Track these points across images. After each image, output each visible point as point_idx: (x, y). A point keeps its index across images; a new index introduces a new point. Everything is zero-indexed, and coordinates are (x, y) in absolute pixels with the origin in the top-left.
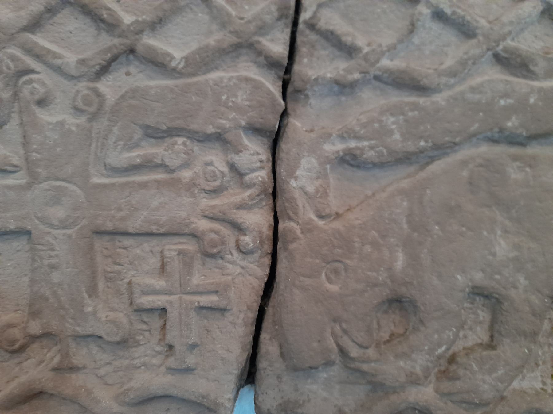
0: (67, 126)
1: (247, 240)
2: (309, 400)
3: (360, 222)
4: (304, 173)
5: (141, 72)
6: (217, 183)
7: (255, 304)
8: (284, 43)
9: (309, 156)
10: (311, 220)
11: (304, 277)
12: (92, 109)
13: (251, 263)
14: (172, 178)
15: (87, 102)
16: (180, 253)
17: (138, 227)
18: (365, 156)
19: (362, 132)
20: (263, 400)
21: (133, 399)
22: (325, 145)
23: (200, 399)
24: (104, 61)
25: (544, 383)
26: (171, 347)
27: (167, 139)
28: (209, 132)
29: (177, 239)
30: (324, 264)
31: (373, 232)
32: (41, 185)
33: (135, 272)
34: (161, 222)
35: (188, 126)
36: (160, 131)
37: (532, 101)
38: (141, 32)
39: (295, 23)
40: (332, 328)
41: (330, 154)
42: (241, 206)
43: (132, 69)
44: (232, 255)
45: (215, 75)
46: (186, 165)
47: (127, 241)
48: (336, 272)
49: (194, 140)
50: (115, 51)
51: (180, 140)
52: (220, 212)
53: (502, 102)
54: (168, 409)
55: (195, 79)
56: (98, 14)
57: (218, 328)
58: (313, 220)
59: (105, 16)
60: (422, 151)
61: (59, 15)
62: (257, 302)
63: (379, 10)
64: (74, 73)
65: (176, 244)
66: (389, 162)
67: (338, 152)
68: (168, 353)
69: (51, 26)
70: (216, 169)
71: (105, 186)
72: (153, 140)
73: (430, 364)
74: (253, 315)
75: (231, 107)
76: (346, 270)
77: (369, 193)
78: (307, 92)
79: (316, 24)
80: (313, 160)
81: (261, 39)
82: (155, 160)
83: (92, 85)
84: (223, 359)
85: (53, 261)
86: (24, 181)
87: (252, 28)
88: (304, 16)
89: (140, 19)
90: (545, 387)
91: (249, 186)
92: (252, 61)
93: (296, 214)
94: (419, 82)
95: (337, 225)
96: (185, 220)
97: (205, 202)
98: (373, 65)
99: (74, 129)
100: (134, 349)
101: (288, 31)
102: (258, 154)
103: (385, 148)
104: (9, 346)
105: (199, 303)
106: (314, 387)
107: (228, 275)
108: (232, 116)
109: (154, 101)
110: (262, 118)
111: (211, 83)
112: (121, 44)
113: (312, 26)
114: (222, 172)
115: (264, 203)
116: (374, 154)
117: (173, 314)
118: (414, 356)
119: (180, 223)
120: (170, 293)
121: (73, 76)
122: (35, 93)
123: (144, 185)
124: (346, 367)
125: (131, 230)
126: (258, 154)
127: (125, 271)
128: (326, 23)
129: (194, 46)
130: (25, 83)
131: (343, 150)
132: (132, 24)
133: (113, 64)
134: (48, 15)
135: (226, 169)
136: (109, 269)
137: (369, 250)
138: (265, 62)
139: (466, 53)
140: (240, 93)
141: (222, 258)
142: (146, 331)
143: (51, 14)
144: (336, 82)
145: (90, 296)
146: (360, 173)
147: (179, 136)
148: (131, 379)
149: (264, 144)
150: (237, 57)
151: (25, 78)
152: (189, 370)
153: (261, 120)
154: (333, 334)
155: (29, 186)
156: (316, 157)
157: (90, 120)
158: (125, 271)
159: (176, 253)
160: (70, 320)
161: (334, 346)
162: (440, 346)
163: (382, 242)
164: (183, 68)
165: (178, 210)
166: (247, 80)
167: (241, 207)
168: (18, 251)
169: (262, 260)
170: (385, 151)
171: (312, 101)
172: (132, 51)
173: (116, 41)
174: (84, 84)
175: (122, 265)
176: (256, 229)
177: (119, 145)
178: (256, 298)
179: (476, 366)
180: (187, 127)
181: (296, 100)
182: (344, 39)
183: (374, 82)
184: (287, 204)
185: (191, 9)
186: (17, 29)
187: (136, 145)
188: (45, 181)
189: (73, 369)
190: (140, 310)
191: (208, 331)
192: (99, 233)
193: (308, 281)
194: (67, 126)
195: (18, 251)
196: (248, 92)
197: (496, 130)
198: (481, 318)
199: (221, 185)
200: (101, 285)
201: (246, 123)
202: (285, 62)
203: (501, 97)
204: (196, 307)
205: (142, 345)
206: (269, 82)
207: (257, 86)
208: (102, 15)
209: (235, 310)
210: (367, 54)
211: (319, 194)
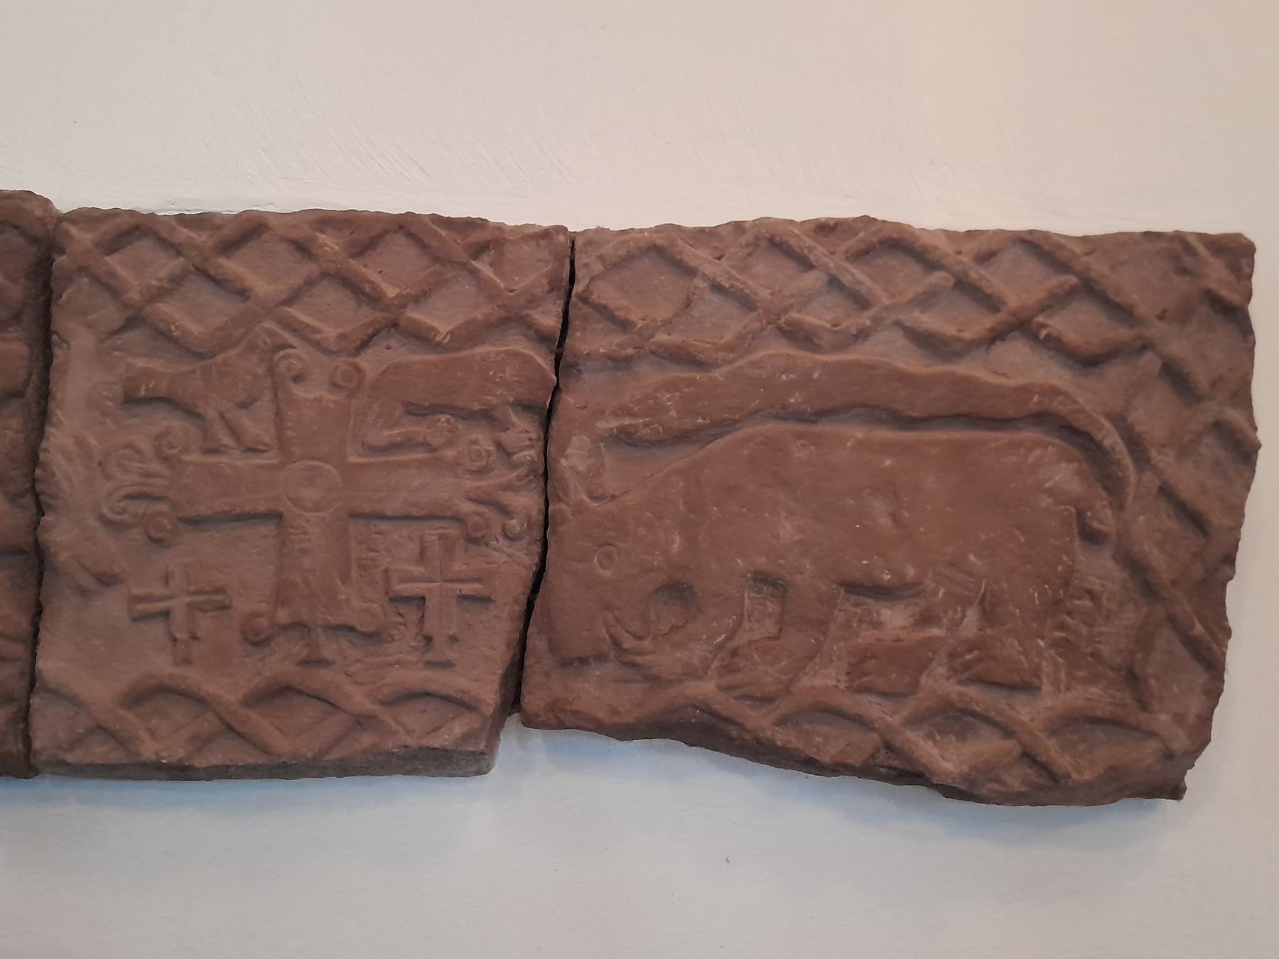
0: (325, 403)
1: (514, 523)
5: (403, 345)
6: (483, 463)
7: (522, 597)
10: (583, 500)
12: (351, 386)
13: (519, 551)
16: (441, 537)
18: (639, 434)
19: (636, 409)
25: (838, 681)
26: (429, 639)
27: (429, 417)
28: (475, 409)
29: (438, 524)
30: (595, 548)
31: (648, 513)
32: (295, 465)
37: (816, 376)
38: (405, 306)
39: (569, 296)
43: (393, 343)
44: (497, 540)
45: (481, 350)
46: (449, 443)
47: (384, 526)
49: (459, 418)
50: (377, 326)
51: (444, 418)
53: (784, 377)
54: (424, 711)
55: (463, 354)
60: (700, 429)
63: (656, 282)
65: (437, 529)
66: (666, 440)
67: (612, 429)
71: (362, 465)
72: (414, 418)
73: (709, 656)
74: (519, 609)
77: (648, 474)
80: (585, 438)
81: (531, 312)
83: (351, 360)
86: (275, 461)
88: (578, 288)
90: (839, 685)
91: (515, 466)
92: (522, 335)
93: (566, 494)
94: (695, 357)
95: (611, 506)
96: (447, 501)
97: (469, 483)
98: (648, 339)
99: (331, 406)
101: (561, 303)
102: (527, 432)
103: (662, 425)
105: (460, 591)
106: (587, 686)
107: (494, 563)
110: (531, 394)
111: (478, 357)
112: (384, 318)
113: (585, 299)
114: (488, 451)
116: (649, 431)
117: (431, 603)
118: (691, 645)
124: (622, 663)
125: (389, 513)
126: (527, 432)
127: (380, 558)
128: (599, 297)
129: (460, 320)
130: (283, 358)
131: (617, 428)
132: (397, 296)
135: (492, 448)
137: (644, 533)
139: (745, 328)
140: (508, 369)
141: (487, 545)
144: (608, 357)
145: (344, 583)
147: (442, 413)
149: (535, 422)
151: (281, 353)
153: (530, 396)
155: (281, 466)
157: (349, 396)
160: (322, 609)
161: (607, 636)
162: (719, 635)
163: (657, 524)
164: (448, 343)
166: (516, 354)
167: (508, 487)
169: (531, 547)
170: (661, 429)
171: (584, 376)
172: (395, 325)
174: (343, 359)
175: (378, 552)
176: (524, 511)
177: (378, 422)
179: (758, 657)
182: (617, 313)
187: (396, 424)
189: (321, 662)
190: (397, 599)
191: (469, 625)
192: (354, 515)
194: (325, 403)
196: (517, 367)
197: (778, 406)
198: (770, 610)
199: (486, 466)
200: (355, 573)
203: (783, 373)
204: (458, 596)
205: (397, 640)
206: (540, 356)
207: (527, 360)
211: (592, 474)
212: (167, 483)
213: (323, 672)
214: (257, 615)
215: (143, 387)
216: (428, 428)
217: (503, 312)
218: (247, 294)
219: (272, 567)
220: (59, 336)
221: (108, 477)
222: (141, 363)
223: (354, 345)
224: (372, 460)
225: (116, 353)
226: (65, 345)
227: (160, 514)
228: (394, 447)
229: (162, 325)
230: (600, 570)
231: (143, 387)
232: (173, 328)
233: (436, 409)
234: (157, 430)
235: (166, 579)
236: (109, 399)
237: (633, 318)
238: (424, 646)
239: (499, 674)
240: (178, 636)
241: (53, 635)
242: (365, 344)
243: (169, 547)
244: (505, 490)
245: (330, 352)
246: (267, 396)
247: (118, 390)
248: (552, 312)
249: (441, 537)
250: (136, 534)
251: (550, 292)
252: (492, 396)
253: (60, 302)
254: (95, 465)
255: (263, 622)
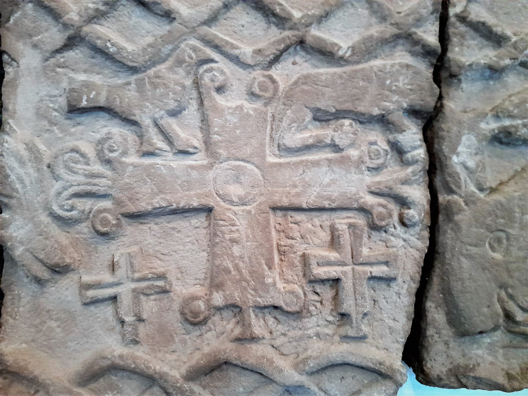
0: (245, 110)
2: (479, 364)
3: (518, 194)
4: (465, 150)
5: (306, 61)
6: (381, 161)
7: (417, 275)
8: (435, 35)
9: (468, 134)
10: (474, 192)
11: (470, 245)
12: (268, 95)
13: (412, 236)
14: (342, 157)
15: (263, 87)
16: (351, 226)
17: (312, 202)
18: (519, 133)
20: (432, 367)
21: (313, 367)
22: (482, 123)
23: (378, 365)
24: (278, 51)
29: (345, 214)
30: (488, 234)
32: (222, 165)
33: (307, 245)
34: (333, 198)
35: (356, 108)
36: (328, 114)
38: (310, 24)
40: (499, 295)
41: (486, 132)
42: (406, 181)
43: (298, 59)
44: (395, 228)
45: (377, 63)
46: (352, 145)
47: (299, 217)
48: (499, 240)
49: (358, 122)
50: (288, 42)
51: (347, 122)
52: (387, 188)
55: (360, 66)
56: (272, 8)
57: (385, 298)
58: (476, 193)
59: (278, 10)
61: (233, 11)
62: (419, 273)
63: (520, 5)
64: (250, 61)
67: (493, 130)
68: (340, 322)
69: (224, 21)
70: (379, 148)
71: (280, 165)
75: (394, 91)
76: (508, 239)
78: (461, 77)
79: (467, 17)
80: (473, 138)
82: (326, 140)
83: (266, 73)
84: (390, 328)
85: (235, 235)
86: (205, 162)
87: (411, 20)
88: (452, 11)
89: (310, 13)
92: (406, 51)
93: (459, 187)
97: (369, 179)
99: (251, 112)
100: (307, 320)
104: (193, 318)
105: (371, 273)
106: (480, 352)
108: (395, 98)
109: (325, 87)
110: (422, 101)
112: (293, 36)
114: (386, 151)
115: (421, 180)
117: (347, 284)
119: (350, 198)
120: (344, 264)
121: (249, 65)
122: (216, 80)
123: (316, 164)
125: (305, 206)
130: (206, 71)
131: (498, 128)
132: (303, 17)
133: (284, 53)
134: (223, 11)
135: (387, 147)
136: (282, 243)
138: (422, 51)
140: (401, 78)
141: (386, 232)
142: (318, 301)
143: (226, 9)
146: (509, 151)
147: (345, 118)
148: (306, 350)
149: (418, 125)
150: (394, 47)
151: (205, 67)
152: (363, 338)
154: (500, 300)
155: (211, 166)
156: (476, 135)
157: (266, 105)
158: (297, 244)
159: (346, 227)
160: (251, 292)
164: (350, 56)
165: (348, 186)
166: (408, 66)
167: (405, 182)
168: (196, 228)
171: (464, 85)
172: (301, 42)
173: (287, 33)
177: (294, 126)
178: (418, 269)
180: (354, 110)
181: (449, 85)
182: (494, 29)
183: (519, 68)
184: (449, 179)
185: (352, 5)
186: (198, 23)
188: (225, 161)
189: (254, 339)
191: (374, 301)
192: (275, 209)
193: (474, 250)
195: (196, 228)
196: (410, 77)
201: (408, 105)
202: (439, 50)
208: (276, 10)
209: (400, 280)
210: (516, 42)
211: (480, 169)
212: (110, 183)
213: (254, 346)
214: (194, 298)
215: (85, 98)
216: (335, 131)
217: (396, 30)
218: (173, 16)
219: (205, 254)
220: (9, 56)
221: (57, 178)
222: (82, 77)
223: (268, 59)
224: (288, 160)
225: (59, 70)
226: (15, 64)
227: (105, 210)
228: (307, 148)
229: (99, 42)
230: (491, 253)
231: (85, 98)
232: (109, 45)
233: (339, 115)
234: (98, 136)
235: (113, 267)
236: (56, 110)
237: (509, 33)
238: (338, 321)
239: (402, 342)
240: (127, 319)
241: (15, 319)
242: (277, 59)
243: (113, 239)
244: (403, 184)
245: (245, 66)
246: (194, 106)
247: (62, 101)
248: (431, 31)
249: (351, 226)
250: (84, 228)
251: (432, 13)
252: (389, 102)
253: (7, 25)
254: (45, 168)
255: (201, 305)
